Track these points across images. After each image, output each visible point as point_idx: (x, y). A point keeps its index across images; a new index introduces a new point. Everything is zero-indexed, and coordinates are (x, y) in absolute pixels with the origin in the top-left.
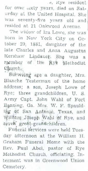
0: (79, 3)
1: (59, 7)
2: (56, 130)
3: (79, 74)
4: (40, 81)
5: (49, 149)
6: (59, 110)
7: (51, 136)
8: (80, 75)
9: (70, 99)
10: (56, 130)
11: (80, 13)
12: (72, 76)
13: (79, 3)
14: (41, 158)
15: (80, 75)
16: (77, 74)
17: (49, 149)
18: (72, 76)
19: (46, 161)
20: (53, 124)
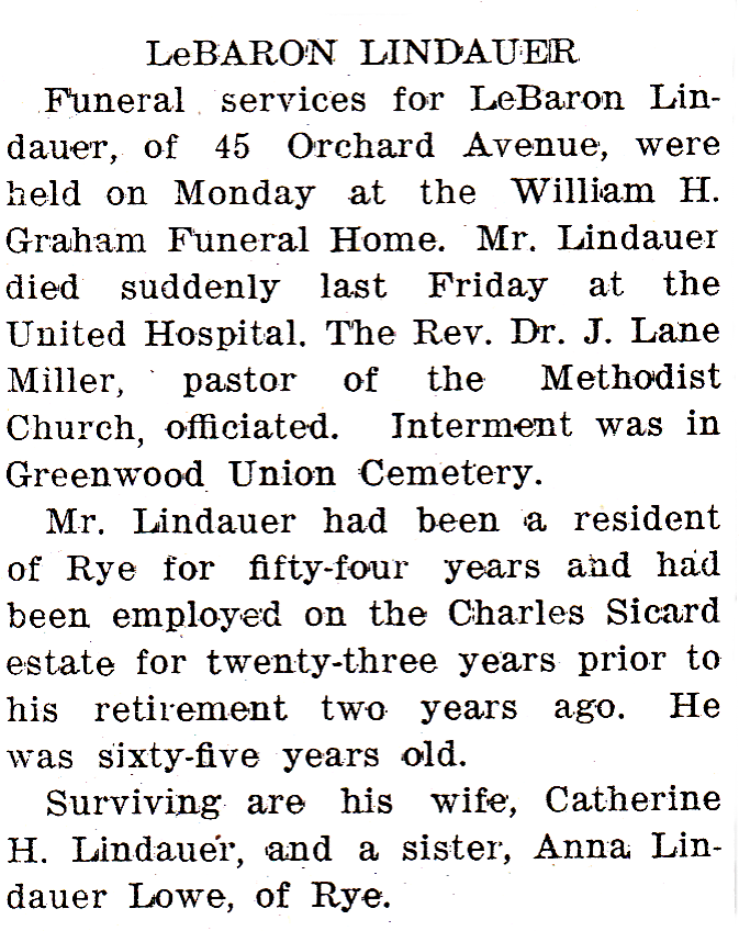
0: (655, 519)
1: (675, 369)
2: (698, 147)
3: (501, 228)
4: (479, 429)
5: (319, 428)
6: (329, 323)
7: (618, 799)
8: (516, 235)
9: (281, 891)
10: (698, 147)
11: (133, 284)
12: (507, 857)
13: (655, 519)
14: (301, 876)
15: (516, 235)
16: (493, 231)
17: (715, 559)
18: (507, 857)
19: (32, 247)
20: (66, 385)
